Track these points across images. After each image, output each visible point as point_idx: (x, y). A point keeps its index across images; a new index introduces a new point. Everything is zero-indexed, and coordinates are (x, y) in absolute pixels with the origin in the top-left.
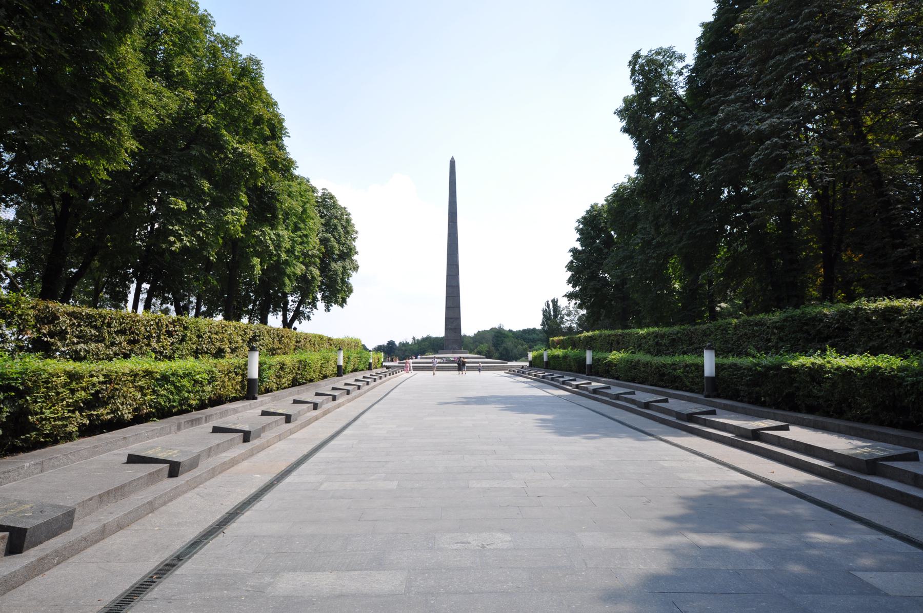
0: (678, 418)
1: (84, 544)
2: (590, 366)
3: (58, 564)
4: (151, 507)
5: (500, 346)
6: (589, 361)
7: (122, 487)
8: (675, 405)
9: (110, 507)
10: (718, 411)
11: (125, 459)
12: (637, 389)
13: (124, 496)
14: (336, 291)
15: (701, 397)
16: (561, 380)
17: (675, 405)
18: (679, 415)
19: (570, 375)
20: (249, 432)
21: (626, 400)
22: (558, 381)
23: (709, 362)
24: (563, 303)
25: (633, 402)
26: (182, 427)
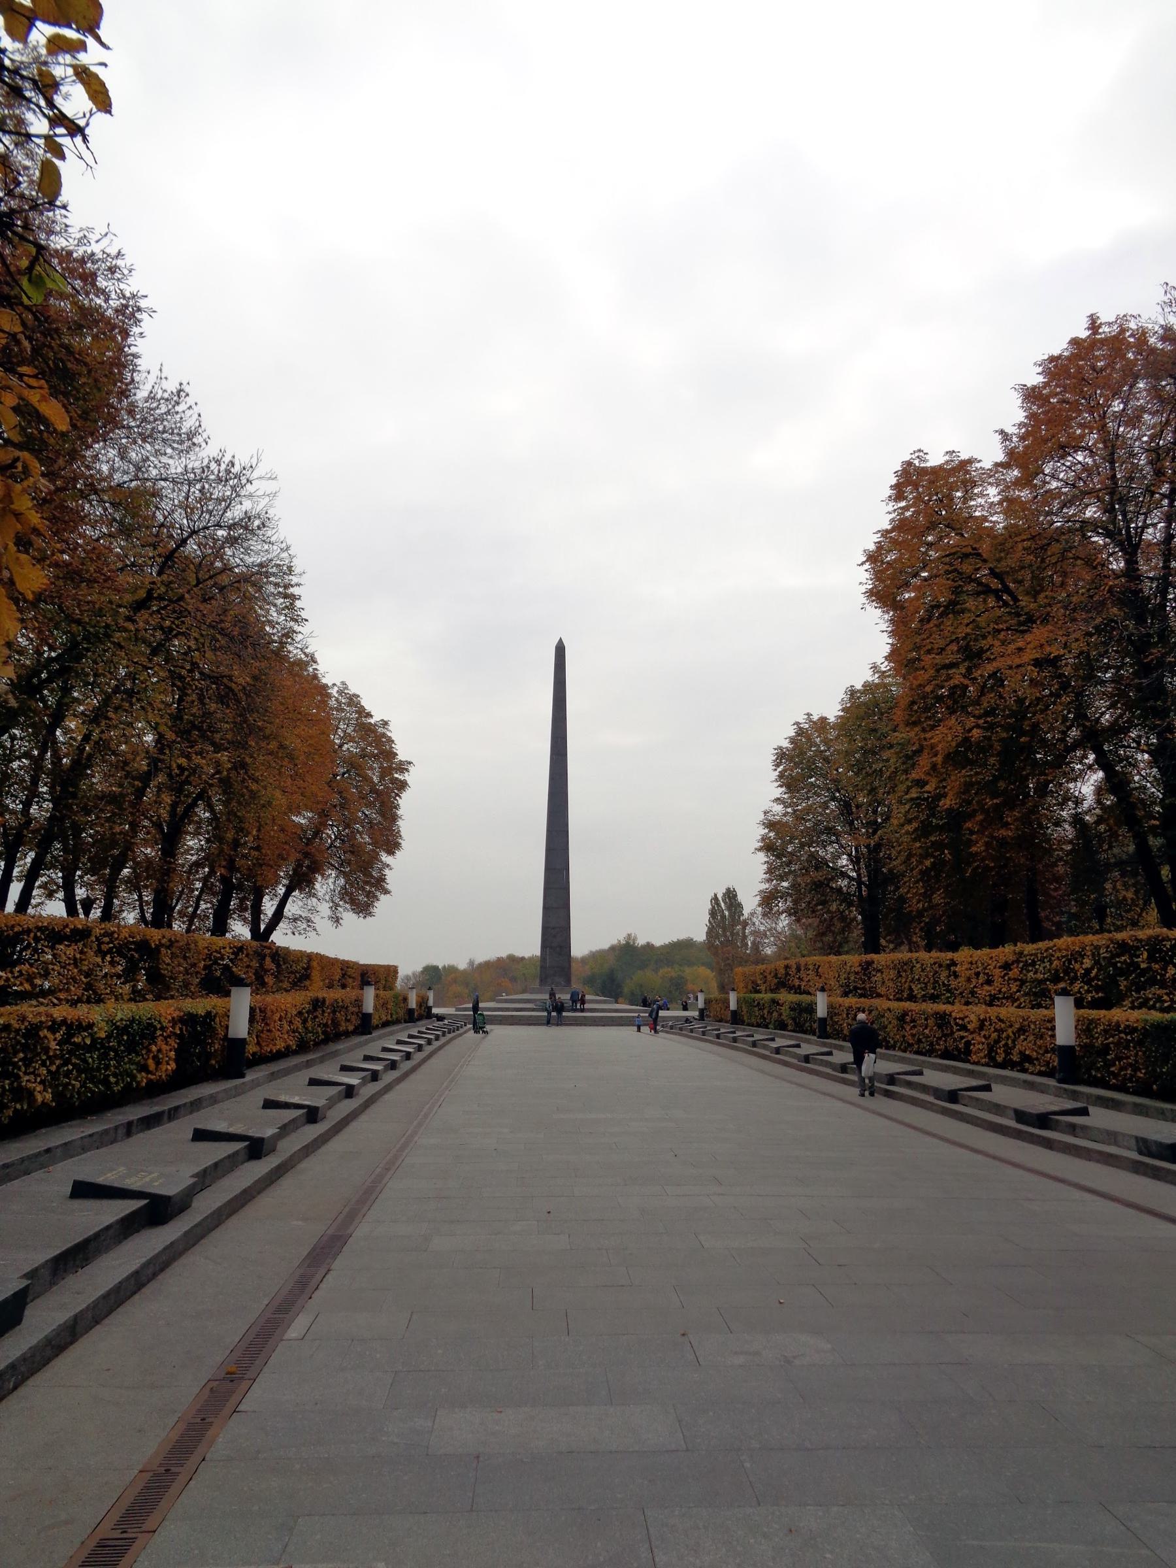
0: (937, 1098)
1: (150, 1271)
2: (823, 1021)
3: (15, 1388)
4: (137, 1282)
5: (638, 984)
6: (821, 1011)
7: (86, 1242)
8: (1002, 1094)
9: (293, 1136)
10: (835, 1052)
11: (68, 1190)
12: (1004, 1080)
13: (87, 1261)
14: (363, 889)
15: (1052, 1082)
16: (774, 1045)
17: (1002, 1094)
18: (937, 1093)
19: (744, 1030)
20: (316, 1109)
21: (909, 1084)
22: (765, 1047)
23: (1065, 1021)
24: (750, 902)
25: (925, 1088)
26: (134, 1129)
